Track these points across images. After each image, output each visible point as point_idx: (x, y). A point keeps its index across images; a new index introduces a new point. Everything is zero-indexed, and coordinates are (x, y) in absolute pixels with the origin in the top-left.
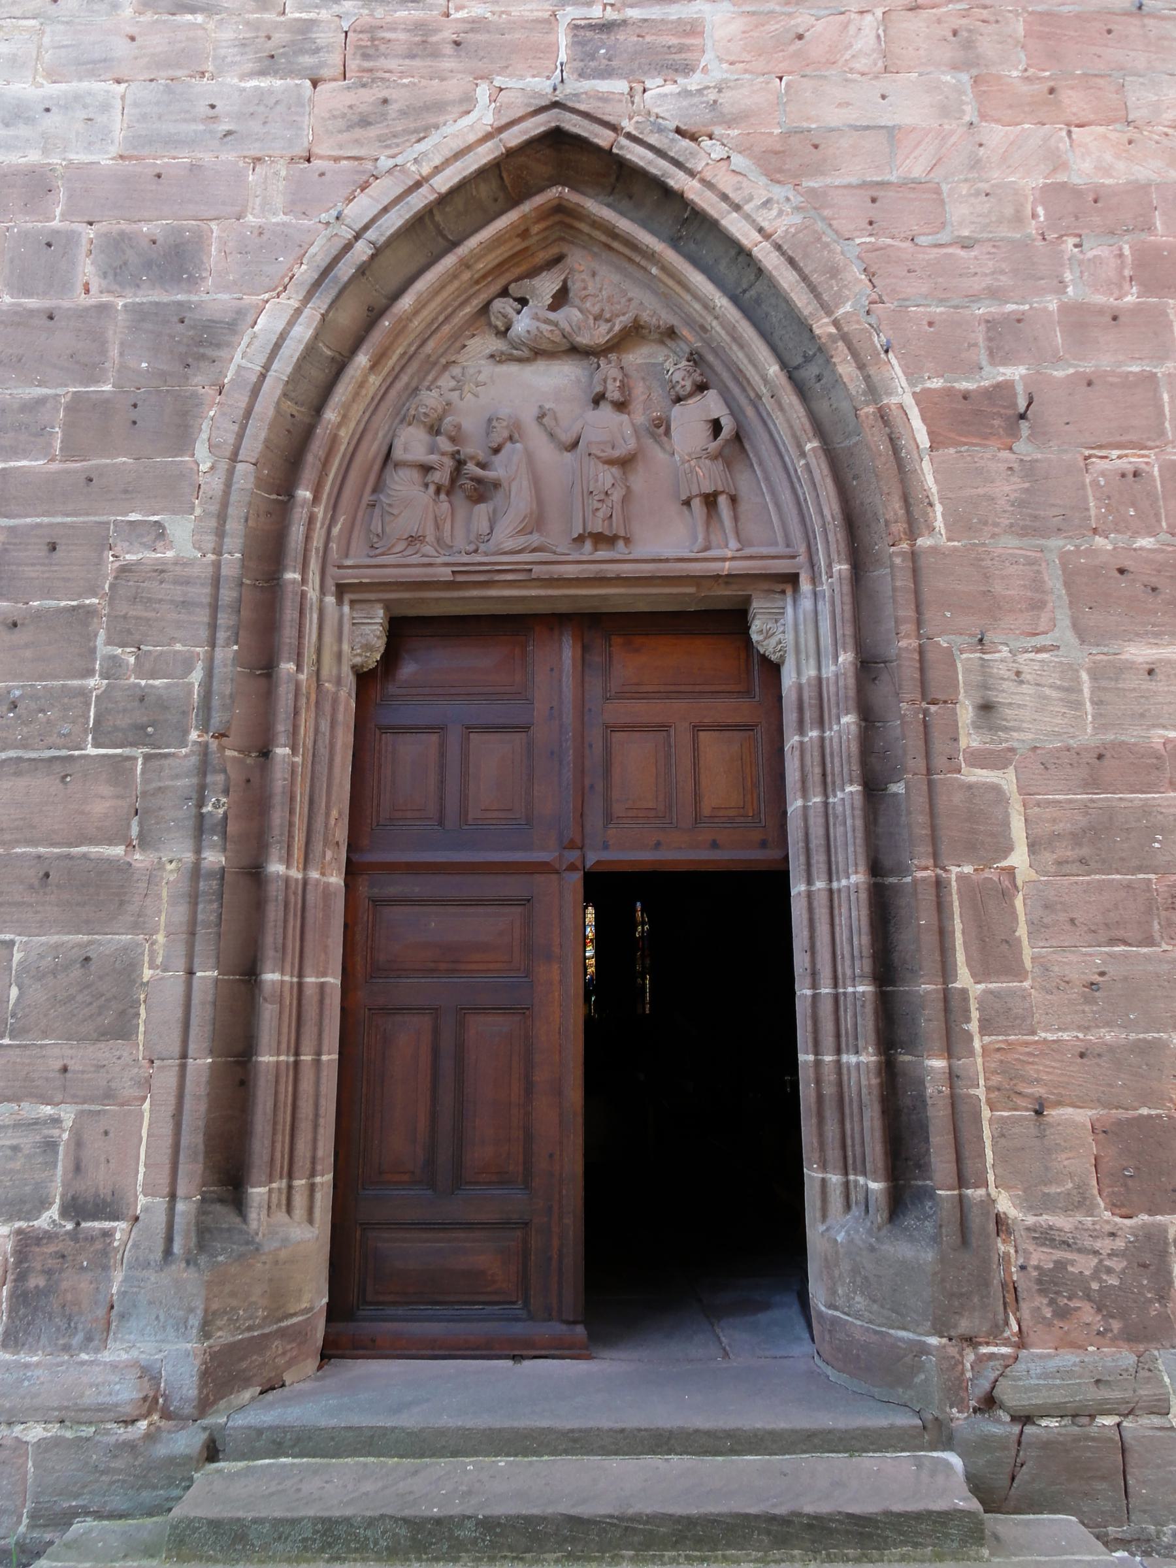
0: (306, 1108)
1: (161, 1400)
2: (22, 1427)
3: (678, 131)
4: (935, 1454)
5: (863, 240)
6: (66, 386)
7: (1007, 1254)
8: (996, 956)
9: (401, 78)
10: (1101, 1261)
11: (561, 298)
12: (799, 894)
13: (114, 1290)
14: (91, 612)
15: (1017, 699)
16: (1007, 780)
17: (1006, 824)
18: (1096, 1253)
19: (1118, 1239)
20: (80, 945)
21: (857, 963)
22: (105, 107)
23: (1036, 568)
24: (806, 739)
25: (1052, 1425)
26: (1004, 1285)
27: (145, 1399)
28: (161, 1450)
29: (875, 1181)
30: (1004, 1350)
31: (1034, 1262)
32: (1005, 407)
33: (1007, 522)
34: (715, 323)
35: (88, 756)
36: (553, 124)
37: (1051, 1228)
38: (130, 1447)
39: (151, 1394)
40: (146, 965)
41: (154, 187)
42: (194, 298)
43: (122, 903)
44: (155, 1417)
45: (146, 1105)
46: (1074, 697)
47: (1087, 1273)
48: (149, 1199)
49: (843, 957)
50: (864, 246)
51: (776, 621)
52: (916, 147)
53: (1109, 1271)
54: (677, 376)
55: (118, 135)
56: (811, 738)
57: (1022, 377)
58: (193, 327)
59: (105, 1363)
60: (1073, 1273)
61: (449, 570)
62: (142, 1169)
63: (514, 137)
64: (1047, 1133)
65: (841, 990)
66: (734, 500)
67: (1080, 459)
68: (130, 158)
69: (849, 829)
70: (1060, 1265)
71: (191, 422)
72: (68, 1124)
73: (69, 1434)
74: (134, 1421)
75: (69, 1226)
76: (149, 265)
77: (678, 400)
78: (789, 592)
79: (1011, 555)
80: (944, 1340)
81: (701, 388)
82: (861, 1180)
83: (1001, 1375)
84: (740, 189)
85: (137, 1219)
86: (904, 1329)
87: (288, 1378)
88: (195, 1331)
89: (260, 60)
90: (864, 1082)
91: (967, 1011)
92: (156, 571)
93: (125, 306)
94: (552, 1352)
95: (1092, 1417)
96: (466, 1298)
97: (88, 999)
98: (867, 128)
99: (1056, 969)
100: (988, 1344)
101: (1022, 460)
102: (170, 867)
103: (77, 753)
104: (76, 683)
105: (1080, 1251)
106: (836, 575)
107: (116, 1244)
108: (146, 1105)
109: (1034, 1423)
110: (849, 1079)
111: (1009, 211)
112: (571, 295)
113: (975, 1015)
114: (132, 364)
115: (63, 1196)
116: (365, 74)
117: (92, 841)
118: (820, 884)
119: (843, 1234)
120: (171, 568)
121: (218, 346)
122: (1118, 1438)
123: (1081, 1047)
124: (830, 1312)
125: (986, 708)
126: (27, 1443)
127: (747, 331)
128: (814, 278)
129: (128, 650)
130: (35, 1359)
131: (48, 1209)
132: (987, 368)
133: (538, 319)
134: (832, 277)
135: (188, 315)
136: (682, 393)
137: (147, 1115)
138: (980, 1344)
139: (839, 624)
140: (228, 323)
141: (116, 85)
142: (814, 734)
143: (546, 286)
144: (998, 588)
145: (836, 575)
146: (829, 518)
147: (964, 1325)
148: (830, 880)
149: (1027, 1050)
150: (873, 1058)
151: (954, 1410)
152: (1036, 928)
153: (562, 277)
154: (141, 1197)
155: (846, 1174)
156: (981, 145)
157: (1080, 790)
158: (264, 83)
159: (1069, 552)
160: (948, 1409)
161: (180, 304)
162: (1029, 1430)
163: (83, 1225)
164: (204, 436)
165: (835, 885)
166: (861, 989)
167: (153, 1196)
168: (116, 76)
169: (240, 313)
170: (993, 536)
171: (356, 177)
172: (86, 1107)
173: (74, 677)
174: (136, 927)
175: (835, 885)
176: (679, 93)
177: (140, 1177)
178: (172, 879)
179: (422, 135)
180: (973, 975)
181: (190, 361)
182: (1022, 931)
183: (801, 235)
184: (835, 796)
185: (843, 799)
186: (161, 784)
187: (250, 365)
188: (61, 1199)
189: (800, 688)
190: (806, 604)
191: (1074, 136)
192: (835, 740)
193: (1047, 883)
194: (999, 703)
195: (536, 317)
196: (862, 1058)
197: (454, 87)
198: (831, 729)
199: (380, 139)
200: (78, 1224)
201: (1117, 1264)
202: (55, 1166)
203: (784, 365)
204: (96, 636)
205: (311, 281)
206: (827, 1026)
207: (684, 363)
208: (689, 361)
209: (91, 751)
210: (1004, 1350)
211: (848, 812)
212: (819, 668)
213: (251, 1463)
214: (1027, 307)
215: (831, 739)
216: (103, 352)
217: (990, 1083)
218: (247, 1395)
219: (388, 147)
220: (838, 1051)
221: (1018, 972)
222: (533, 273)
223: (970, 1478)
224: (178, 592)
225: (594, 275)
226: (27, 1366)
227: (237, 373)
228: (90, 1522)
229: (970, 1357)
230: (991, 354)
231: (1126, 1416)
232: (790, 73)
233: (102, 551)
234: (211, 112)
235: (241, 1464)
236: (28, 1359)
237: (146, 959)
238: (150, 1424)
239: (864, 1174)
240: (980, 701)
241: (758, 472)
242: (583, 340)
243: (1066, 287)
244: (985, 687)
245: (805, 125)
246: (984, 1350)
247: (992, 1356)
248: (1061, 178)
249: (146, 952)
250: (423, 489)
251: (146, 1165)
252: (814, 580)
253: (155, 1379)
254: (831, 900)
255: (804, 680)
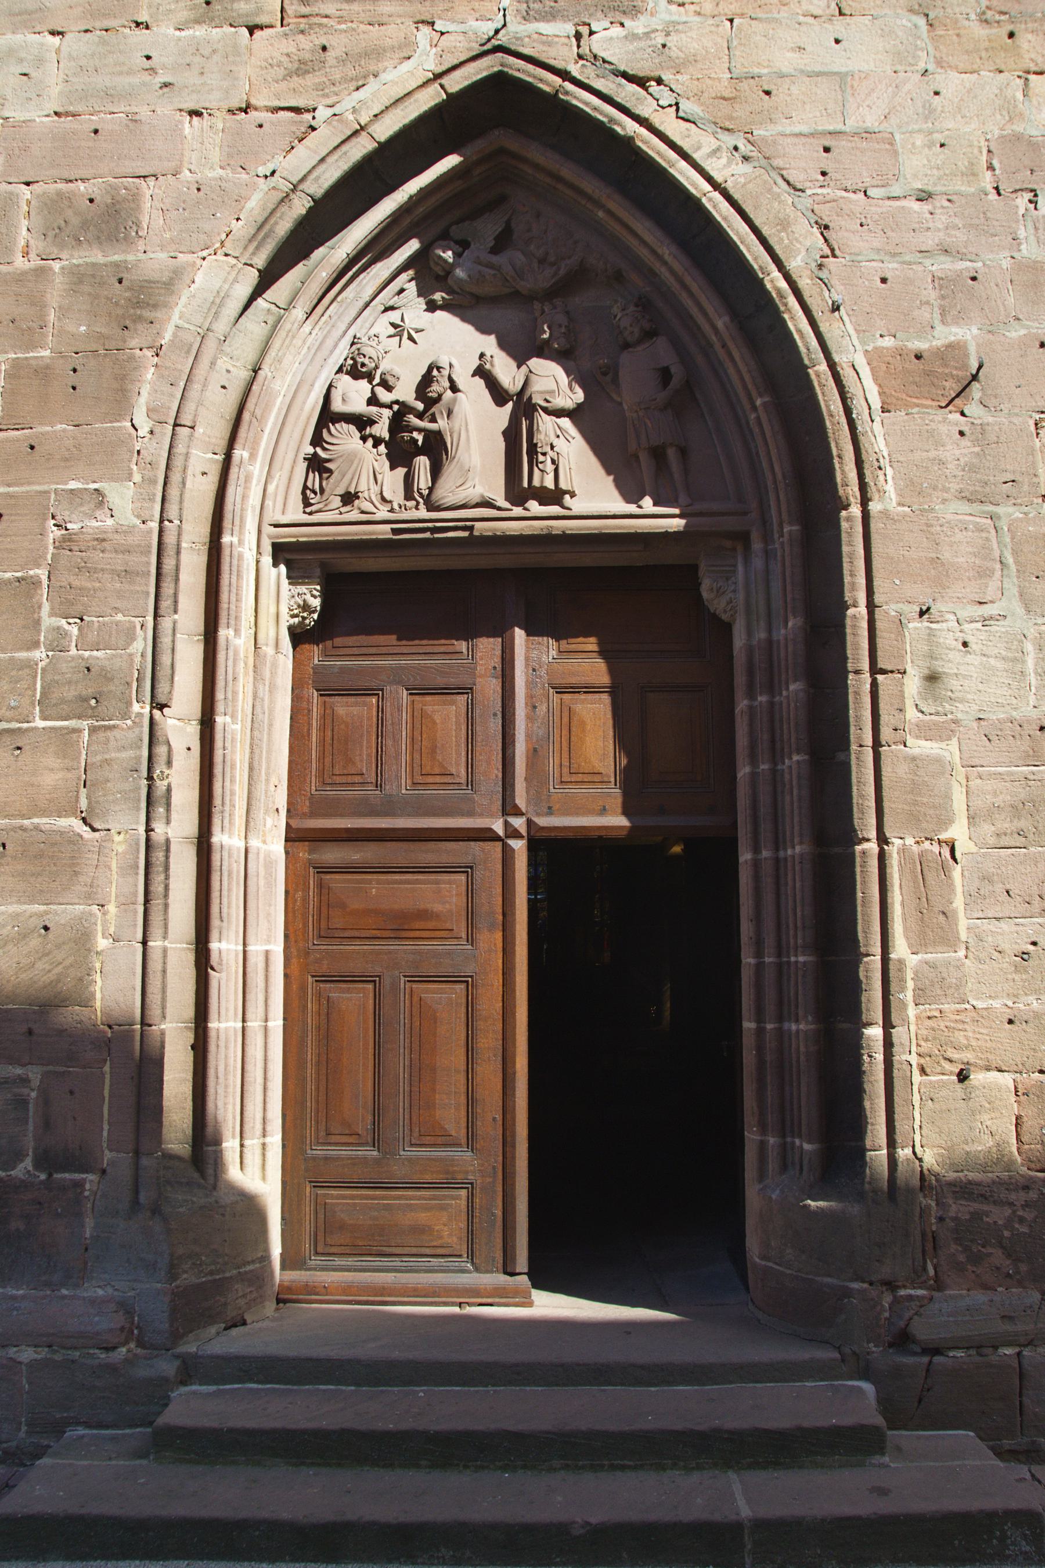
0: (255, 1073)
1: (136, 1332)
2: (15, 1349)
3: (625, 75)
4: (850, 1383)
5: (814, 191)
6: (6, 353)
7: (929, 1207)
8: (936, 926)
9: (339, 23)
10: (1014, 1212)
11: (502, 242)
12: (746, 861)
13: (88, 1235)
14: (36, 583)
15: (963, 670)
16: (949, 751)
17: (948, 797)
18: (1011, 1204)
19: (1031, 1192)
20: (40, 915)
21: (800, 934)
22: (40, 61)
23: (984, 535)
24: (756, 703)
25: (959, 1355)
26: (923, 1235)
27: (122, 1329)
28: (142, 1372)
29: (809, 1142)
30: (920, 1292)
31: (952, 1214)
32: (956, 368)
33: (957, 487)
34: (663, 270)
35: (36, 728)
36: (496, 69)
37: (970, 1182)
38: (112, 1369)
39: (127, 1326)
40: (100, 934)
41: (91, 144)
42: (130, 258)
43: (76, 873)
44: (132, 1345)
45: (107, 1068)
46: (1019, 667)
47: (1000, 1222)
48: (114, 1154)
49: (788, 926)
50: (816, 198)
51: (727, 579)
52: (869, 94)
53: (1021, 1220)
54: (625, 323)
55: (55, 91)
56: (761, 702)
57: (974, 337)
58: (129, 289)
59: (84, 1298)
60: (988, 1222)
61: (388, 527)
62: (106, 1127)
63: (456, 82)
64: (973, 1095)
65: (785, 959)
66: (683, 452)
67: (1032, 423)
68: (67, 114)
69: (795, 799)
70: (976, 1216)
71: (130, 387)
72: (36, 1082)
73: (57, 1357)
74: (114, 1348)
75: (43, 1177)
76: (85, 225)
77: (626, 346)
78: (740, 549)
79: (961, 521)
80: (865, 1285)
81: (649, 335)
82: (797, 1142)
83: (916, 1314)
84: (688, 136)
85: (104, 1172)
86: (829, 1276)
87: (248, 1318)
88: (163, 1273)
89: (194, 7)
90: (802, 1049)
91: (903, 980)
92: (97, 539)
93: (62, 268)
94: (497, 1300)
95: (996, 1348)
96: (414, 1251)
97: (47, 967)
98: (819, 74)
99: (990, 939)
100: (905, 1287)
101: (973, 423)
102: (118, 838)
103: (25, 725)
104: (23, 655)
105: (995, 1203)
106: (786, 535)
107: (87, 1193)
108: (107, 1068)
109: (942, 1354)
110: (790, 1046)
111: (963, 164)
112: (514, 237)
113: (910, 984)
114: (71, 328)
115: (35, 1149)
116: (302, 20)
117: (44, 813)
118: (765, 854)
119: (778, 1192)
120: (110, 536)
121: (155, 306)
122: (1017, 1365)
123: (1008, 1014)
124: (763, 1263)
125: (932, 678)
126: (20, 1363)
127: (696, 284)
128: (765, 231)
129: (71, 621)
130: (21, 1292)
131: (22, 1161)
132: (940, 328)
133: (480, 264)
134: (784, 229)
135: (125, 275)
136: (629, 339)
137: (108, 1076)
138: (898, 1287)
139: (789, 588)
140: (164, 283)
141: (50, 37)
142: (762, 699)
143: (488, 228)
144: (946, 555)
145: (786, 535)
146: (779, 476)
147: (885, 1271)
148: (777, 850)
149: (958, 1017)
150: (812, 1027)
151: (871, 1345)
152: (973, 898)
153: (506, 218)
154: (107, 1152)
155: (784, 1136)
156: (937, 93)
157: (1020, 763)
158: (199, 32)
159: (1017, 519)
160: (865, 1345)
161: (116, 265)
162: (937, 1359)
163: (55, 1176)
164: (143, 400)
165: (781, 854)
166: (801, 959)
167: (118, 1151)
168: (50, 28)
169: (177, 274)
170: (944, 501)
171: (294, 129)
172: (51, 1068)
173: (20, 649)
174: (89, 897)
175: (781, 854)
176: (626, 37)
177: (105, 1134)
178: (120, 850)
179: (360, 83)
180: (910, 946)
181: (128, 323)
182: (958, 902)
183: (750, 186)
184: (784, 763)
185: (790, 767)
186: (107, 757)
187: (187, 326)
188: (34, 1152)
189: (750, 650)
190: (758, 563)
191: (1031, 85)
192: (784, 705)
193: (984, 855)
194: (944, 673)
195: (478, 262)
196: (801, 1027)
197: (393, 33)
198: (781, 694)
199: (320, 88)
200: (50, 1175)
201: (1029, 1215)
202: (27, 1123)
203: (734, 313)
204: (40, 607)
205: (248, 236)
206: (770, 995)
207: (632, 308)
208: (637, 306)
209: (40, 724)
210: (920, 1292)
211: (794, 783)
212: (770, 631)
213: (221, 1387)
214: (980, 264)
215: (781, 703)
216: (42, 317)
217: (921, 1050)
218: (213, 1330)
219: (327, 96)
220: (780, 1019)
221: (949, 940)
222: (473, 216)
223: (880, 1401)
224: (119, 561)
225: (538, 215)
226: (14, 1298)
227: (175, 335)
228: (81, 1431)
229: (887, 1299)
230: (943, 314)
231: (1025, 1346)
232: (742, 15)
233: (45, 520)
234: (147, 64)
235: (214, 1388)
236: (14, 1292)
237: (99, 928)
238: (129, 1351)
239: (800, 1137)
240: (927, 672)
241: (710, 423)
242: (525, 286)
243: (1019, 244)
244: (932, 656)
245: (756, 71)
246: (902, 1292)
247: (910, 1298)
248: (1019, 128)
249: (99, 922)
250: (361, 442)
251: (109, 1123)
252: (767, 538)
253: (129, 1313)
254: (777, 869)
255: (755, 643)
